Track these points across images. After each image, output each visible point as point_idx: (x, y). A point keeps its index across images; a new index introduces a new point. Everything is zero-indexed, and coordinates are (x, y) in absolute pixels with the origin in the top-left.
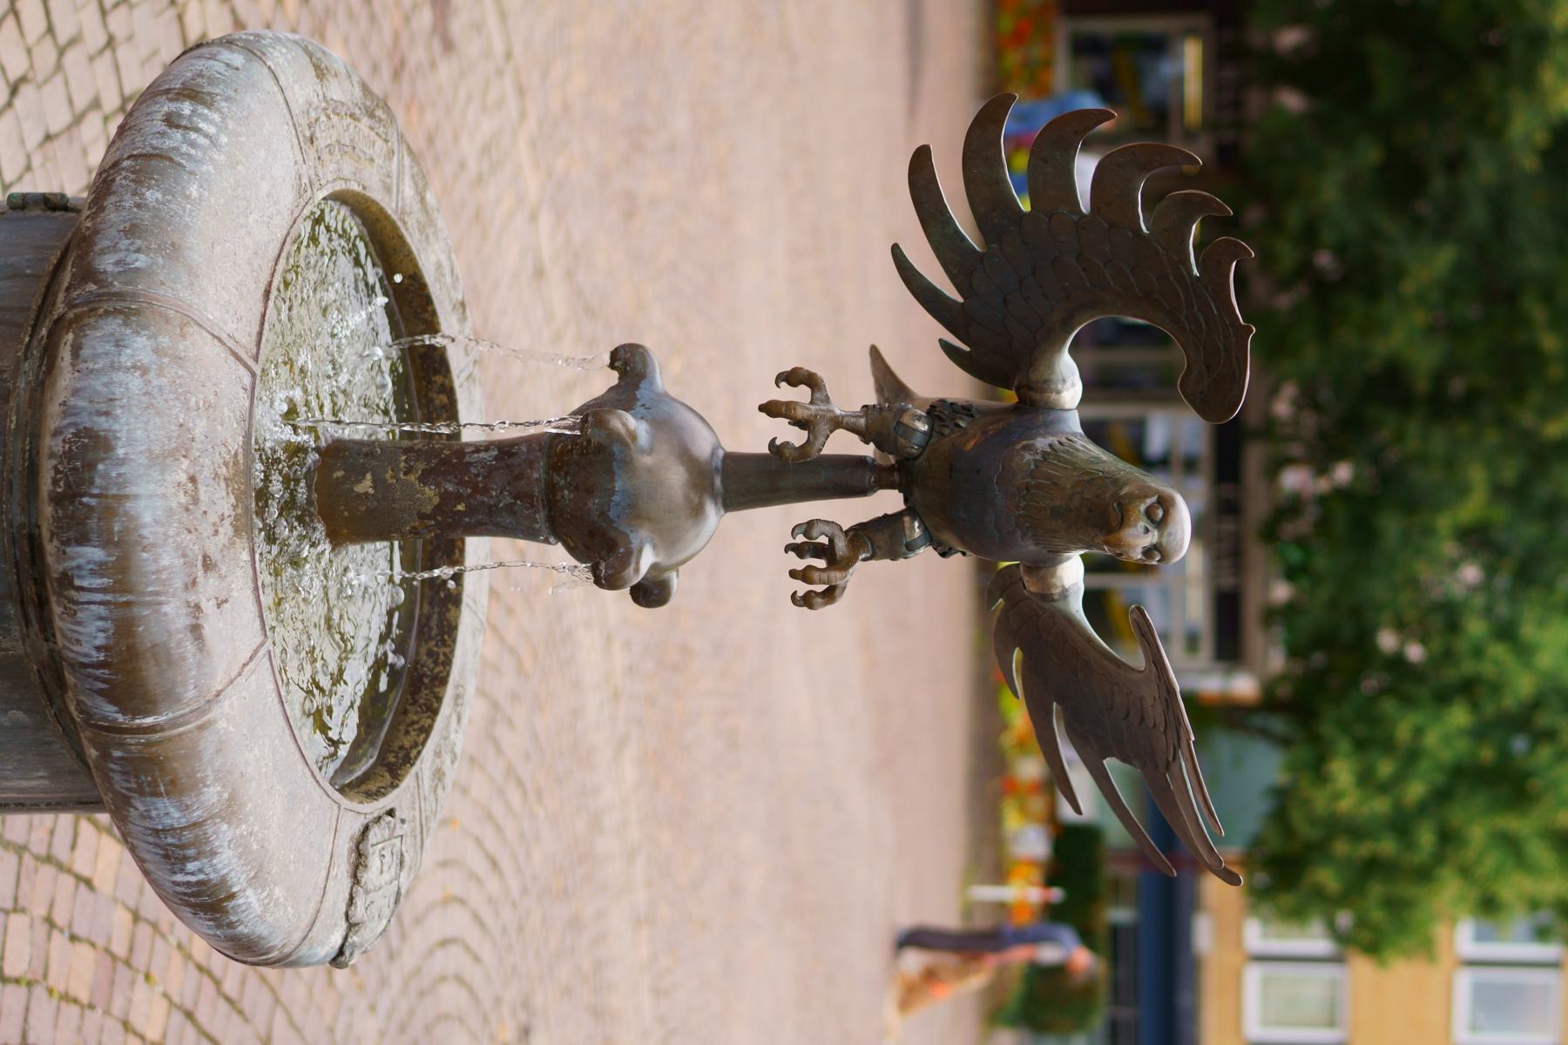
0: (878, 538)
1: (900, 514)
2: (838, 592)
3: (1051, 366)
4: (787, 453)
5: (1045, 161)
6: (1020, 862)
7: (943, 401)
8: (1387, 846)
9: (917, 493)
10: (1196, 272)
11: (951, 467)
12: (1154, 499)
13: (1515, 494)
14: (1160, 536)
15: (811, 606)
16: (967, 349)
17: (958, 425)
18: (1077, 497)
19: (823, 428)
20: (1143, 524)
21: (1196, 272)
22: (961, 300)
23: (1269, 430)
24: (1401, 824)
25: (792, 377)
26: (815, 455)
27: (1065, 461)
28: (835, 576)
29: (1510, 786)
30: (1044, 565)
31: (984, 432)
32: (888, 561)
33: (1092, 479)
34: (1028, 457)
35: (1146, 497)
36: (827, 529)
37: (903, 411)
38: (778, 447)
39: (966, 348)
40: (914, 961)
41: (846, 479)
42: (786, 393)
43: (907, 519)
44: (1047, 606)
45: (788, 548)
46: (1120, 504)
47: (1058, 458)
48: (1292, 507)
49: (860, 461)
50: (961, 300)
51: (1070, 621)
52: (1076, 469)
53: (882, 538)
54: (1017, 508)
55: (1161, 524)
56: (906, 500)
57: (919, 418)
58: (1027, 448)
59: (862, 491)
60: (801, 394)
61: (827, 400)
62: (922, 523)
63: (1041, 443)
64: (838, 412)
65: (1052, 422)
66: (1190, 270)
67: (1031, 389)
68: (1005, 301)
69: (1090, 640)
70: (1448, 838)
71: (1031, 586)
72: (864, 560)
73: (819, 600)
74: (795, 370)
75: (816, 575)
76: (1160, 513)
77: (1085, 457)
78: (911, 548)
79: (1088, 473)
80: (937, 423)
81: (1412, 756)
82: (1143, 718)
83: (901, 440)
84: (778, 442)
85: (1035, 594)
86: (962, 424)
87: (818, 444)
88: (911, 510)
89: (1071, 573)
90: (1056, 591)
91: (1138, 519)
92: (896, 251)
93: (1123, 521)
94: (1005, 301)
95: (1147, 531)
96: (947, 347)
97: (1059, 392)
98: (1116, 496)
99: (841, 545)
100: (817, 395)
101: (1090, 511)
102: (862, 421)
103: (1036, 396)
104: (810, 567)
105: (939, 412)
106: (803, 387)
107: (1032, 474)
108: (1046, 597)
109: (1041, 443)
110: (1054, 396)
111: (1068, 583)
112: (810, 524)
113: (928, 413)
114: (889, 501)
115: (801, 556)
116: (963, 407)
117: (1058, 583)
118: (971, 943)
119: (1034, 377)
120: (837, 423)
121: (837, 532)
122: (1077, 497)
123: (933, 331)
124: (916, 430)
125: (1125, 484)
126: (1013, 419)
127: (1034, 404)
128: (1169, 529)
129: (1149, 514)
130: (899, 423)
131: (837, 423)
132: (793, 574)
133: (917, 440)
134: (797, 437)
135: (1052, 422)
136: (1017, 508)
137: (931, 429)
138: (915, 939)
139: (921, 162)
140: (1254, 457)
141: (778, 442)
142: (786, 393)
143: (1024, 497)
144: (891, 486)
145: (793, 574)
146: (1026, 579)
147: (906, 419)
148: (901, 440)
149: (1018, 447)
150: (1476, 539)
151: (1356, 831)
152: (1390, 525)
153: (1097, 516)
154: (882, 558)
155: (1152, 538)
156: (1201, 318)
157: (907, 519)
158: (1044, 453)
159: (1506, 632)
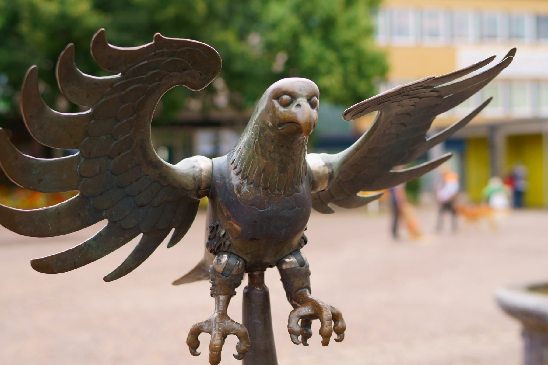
0: (296, 285)
1: (281, 271)
2: (334, 312)
3: (185, 176)
4: (243, 348)
5: (40, 181)
6: (392, 192)
7: (208, 245)
8: (351, 67)
9: (267, 260)
10: (118, 75)
11: (252, 239)
12: (275, 102)
13: (226, 24)
14: (302, 96)
15: (344, 329)
16: (173, 230)
17: (224, 235)
18: (273, 155)
19: (227, 324)
20: (293, 109)
21: (118, 75)
22: (141, 235)
23: (205, 109)
24: (343, 61)
25: (193, 345)
26: (244, 329)
27: (248, 164)
28: (326, 314)
29: (328, 26)
30: (313, 180)
31: (229, 218)
32: (310, 277)
33: (260, 145)
34: (245, 189)
35: (274, 107)
36: (294, 321)
37: (214, 271)
38: (240, 354)
39: (173, 230)
40: (403, 232)
41: (258, 305)
42: (204, 349)
43: (284, 267)
44: (336, 176)
45: (306, 344)
46: (280, 125)
47: (246, 169)
48: (233, 103)
49: (247, 296)
50: (141, 235)
51: (345, 161)
52: (253, 157)
53: (297, 283)
54: (279, 195)
55: (293, 96)
56: (271, 266)
57: (219, 260)
58: (239, 189)
59: (266, 295)
60: (204, 339)
61: (208, 322)
62: (286, 257)
63: (235, 181)
64: (216, 314)
65: (221, 174)
66: (117, 80)
67: (199, 188)
68: (142, 206)
69: (357, 149)
70: (349, 44)
71: (323, 186)
72: (310, 293)
73: (340, 324)
74: (189, 343)
75: (326, 329)
76: (286, 97)
77: (244, 151)
78: (303, 263)
79: (256, 150)
80: (222, 248)
81: (320, 59)
82: (408, 114)
83: (234, 272)
84: (236, 353)
85: (329, 184)
86: (223, 232)
87: (238, 327)
88: (279, 264)
89: (316, 161)
90: (327, 171)
91: (290, 112)
92: (108, 279)
93: (293, 122)
94: (142, 206)
95: (299, 105)
96: (172, 243)
97: (201, 170)
98: (272, 129)
99: (305, 310)
100: (205, 328)
101: (282, 146)
102: (222, 298)
103: (204, 185)
104: (321, 332)
105: (215, 245)
106: (200, 338)
107: (257, 186)
108: (331, 176)
109: (235, 181)
110: (204, 174)
111: (322, 163)
112: (291, 332)
113: (215, 254)
114: (272, 278)
115: (309, 335)
116: (211, 232)
117: (322, 169)
118: (397, 212)
119: (191, 185)
120: (223, 315)
121: (296, 313)
122: (273, 155)
123: (162, 250)
124: (227, 263)
125: (264, 122)
126: (219, 200)
127: (209, 187)
128: (296, 90)
129: (286, 105)
130: (223, 274)
131: (223, 315)
132: (325, 343)
133: (233, 261)
134: (232, 341)
135: (221, 174)
136: (279, 195)
137: (226, 252)
138: (394, 230)
139: (42, 266)
140: (214, 115)
141: (236, 353)
142: (204, 349)
143: (272, 191)
144: (262, 276)
145: (325, 343)
146: (319, 189)
147: (220, 269)
148: (234, 272)
149: (238, 196)
150: (242, 36)
151: (345, 77)
152: (238, 66)
153: (286, 138)
154: (308, 281)
155: (303, 101)
156: (151, 72)
157: (284, 267)
158: (242, 178)
159: (274, 26)
